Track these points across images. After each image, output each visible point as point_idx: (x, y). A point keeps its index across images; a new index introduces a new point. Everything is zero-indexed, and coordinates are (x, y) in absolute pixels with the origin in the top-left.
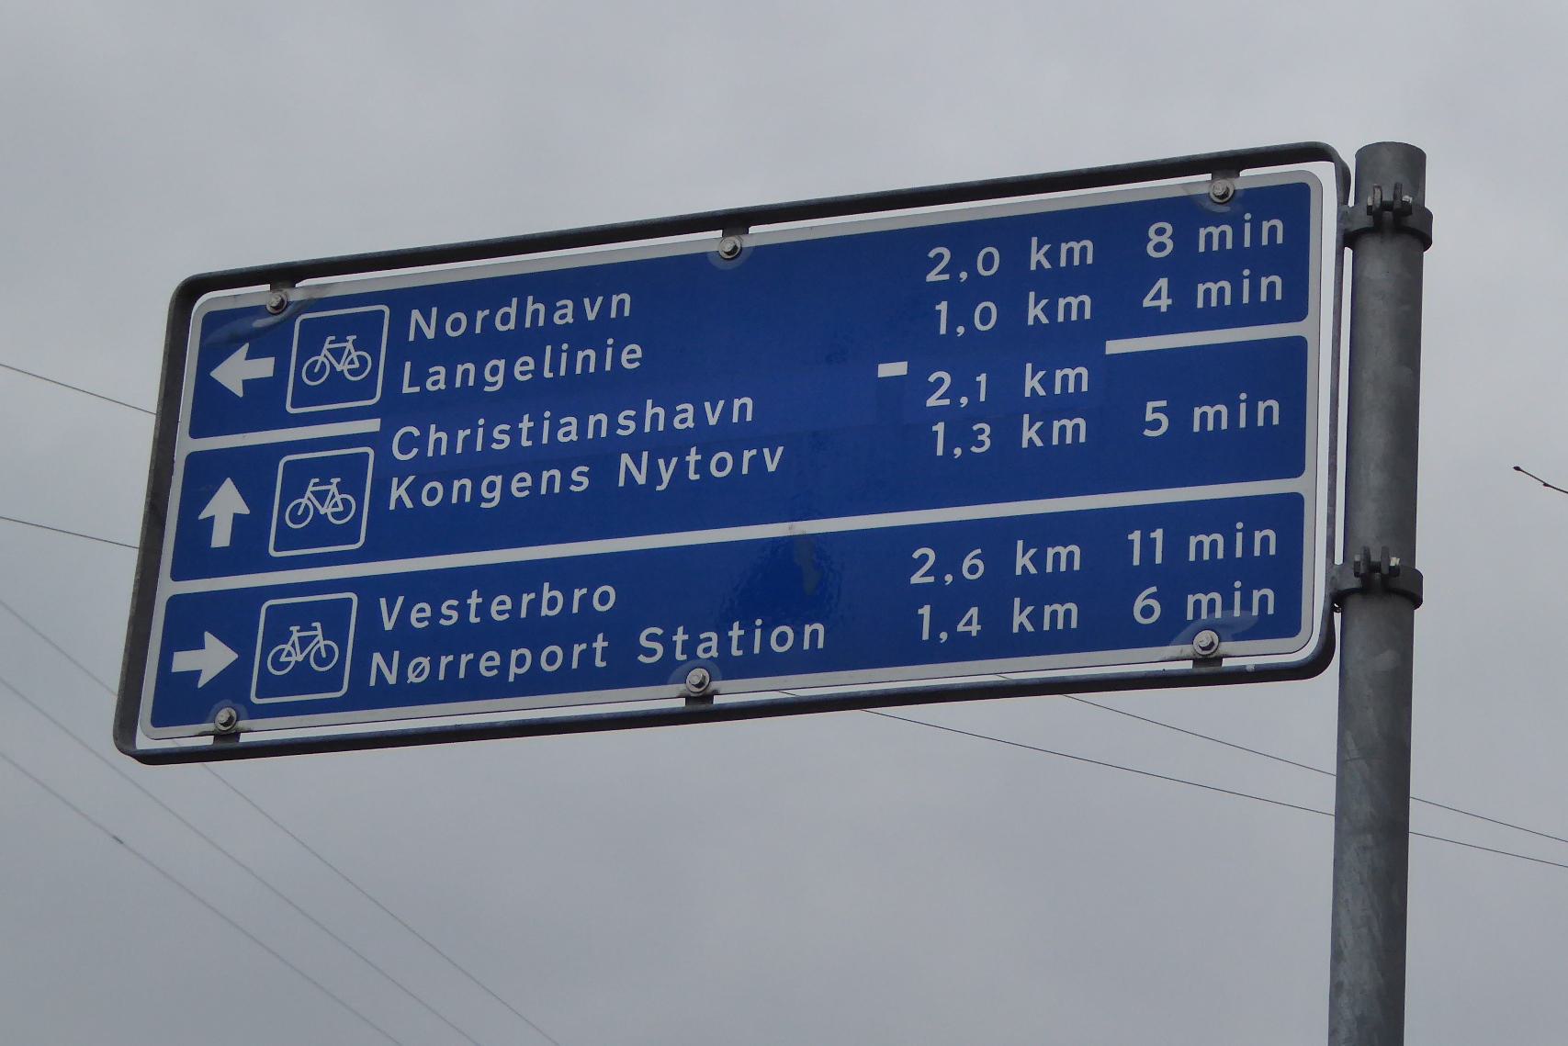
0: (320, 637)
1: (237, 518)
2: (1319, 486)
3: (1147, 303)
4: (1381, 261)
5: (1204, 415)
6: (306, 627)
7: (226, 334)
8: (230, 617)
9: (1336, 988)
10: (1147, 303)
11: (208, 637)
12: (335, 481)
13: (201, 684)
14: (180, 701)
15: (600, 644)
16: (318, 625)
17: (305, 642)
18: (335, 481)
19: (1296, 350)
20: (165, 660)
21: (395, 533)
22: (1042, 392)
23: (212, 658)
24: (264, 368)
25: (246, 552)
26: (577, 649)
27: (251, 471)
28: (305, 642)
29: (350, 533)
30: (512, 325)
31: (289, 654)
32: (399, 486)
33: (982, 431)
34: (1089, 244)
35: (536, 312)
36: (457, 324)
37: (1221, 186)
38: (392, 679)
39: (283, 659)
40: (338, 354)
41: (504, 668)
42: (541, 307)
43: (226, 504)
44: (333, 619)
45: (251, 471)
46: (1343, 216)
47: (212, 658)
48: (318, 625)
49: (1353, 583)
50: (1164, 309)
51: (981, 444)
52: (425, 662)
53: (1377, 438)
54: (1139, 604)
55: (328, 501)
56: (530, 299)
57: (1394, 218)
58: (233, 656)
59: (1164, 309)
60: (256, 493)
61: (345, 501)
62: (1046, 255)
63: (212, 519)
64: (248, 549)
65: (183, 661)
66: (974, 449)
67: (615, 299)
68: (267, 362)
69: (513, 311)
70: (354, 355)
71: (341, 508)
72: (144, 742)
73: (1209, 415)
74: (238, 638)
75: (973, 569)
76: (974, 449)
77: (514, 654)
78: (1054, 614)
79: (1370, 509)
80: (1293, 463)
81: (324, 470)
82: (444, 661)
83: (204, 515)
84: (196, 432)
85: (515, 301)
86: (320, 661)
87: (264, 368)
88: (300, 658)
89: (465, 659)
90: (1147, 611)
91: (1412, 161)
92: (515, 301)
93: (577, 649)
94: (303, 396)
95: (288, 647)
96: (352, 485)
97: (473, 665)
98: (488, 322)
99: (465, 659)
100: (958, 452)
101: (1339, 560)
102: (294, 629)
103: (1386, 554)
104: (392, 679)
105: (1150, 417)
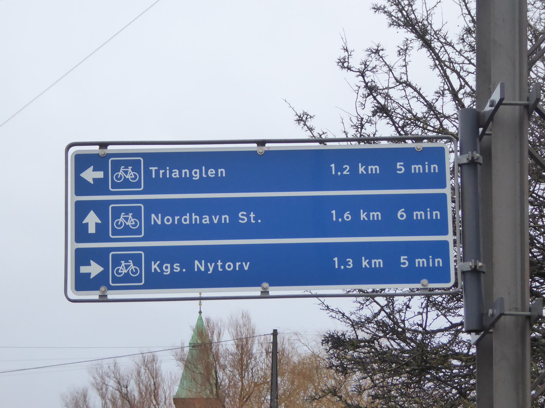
0: (132, 265)
7: (82, 162)
8: (100, 256)
11: (92, 182)
14: (83, 283)
18: (131, 214)
21: (153, 233)
23: (94, 269)
24: (100, 175)
25: (101, 234)
27: (100, 209)
28: (127, 267)
29: (138, 231)
30: (188, 222)
32: (155, 264)
33: (349, 261)
35: (196, 219)
36: (168, 220)
38: (159, 222)
39: (120, 271)
43: (92, 220)
45: (100, 209)
47: (94, 269)
48: (131, 261)
51: (350, 265)
54: (399, 214)
56: (193, 214)
64: (101, 234)
65: (84, 269)
66: (347, 267)
68: (99, 174)
69: (188, 217)
73: (418, 214)
74: (102, 262)
75: (348, 217)
76: (347, 267)
81: (127, 210)
85: (188, 214)
87: (100, 175)
88: (126, 271)
90: (402, 216)
92: (188, 214)
95: (121, 268)
98: (179, 220)
102: (123, 262)
104: (159, 222)
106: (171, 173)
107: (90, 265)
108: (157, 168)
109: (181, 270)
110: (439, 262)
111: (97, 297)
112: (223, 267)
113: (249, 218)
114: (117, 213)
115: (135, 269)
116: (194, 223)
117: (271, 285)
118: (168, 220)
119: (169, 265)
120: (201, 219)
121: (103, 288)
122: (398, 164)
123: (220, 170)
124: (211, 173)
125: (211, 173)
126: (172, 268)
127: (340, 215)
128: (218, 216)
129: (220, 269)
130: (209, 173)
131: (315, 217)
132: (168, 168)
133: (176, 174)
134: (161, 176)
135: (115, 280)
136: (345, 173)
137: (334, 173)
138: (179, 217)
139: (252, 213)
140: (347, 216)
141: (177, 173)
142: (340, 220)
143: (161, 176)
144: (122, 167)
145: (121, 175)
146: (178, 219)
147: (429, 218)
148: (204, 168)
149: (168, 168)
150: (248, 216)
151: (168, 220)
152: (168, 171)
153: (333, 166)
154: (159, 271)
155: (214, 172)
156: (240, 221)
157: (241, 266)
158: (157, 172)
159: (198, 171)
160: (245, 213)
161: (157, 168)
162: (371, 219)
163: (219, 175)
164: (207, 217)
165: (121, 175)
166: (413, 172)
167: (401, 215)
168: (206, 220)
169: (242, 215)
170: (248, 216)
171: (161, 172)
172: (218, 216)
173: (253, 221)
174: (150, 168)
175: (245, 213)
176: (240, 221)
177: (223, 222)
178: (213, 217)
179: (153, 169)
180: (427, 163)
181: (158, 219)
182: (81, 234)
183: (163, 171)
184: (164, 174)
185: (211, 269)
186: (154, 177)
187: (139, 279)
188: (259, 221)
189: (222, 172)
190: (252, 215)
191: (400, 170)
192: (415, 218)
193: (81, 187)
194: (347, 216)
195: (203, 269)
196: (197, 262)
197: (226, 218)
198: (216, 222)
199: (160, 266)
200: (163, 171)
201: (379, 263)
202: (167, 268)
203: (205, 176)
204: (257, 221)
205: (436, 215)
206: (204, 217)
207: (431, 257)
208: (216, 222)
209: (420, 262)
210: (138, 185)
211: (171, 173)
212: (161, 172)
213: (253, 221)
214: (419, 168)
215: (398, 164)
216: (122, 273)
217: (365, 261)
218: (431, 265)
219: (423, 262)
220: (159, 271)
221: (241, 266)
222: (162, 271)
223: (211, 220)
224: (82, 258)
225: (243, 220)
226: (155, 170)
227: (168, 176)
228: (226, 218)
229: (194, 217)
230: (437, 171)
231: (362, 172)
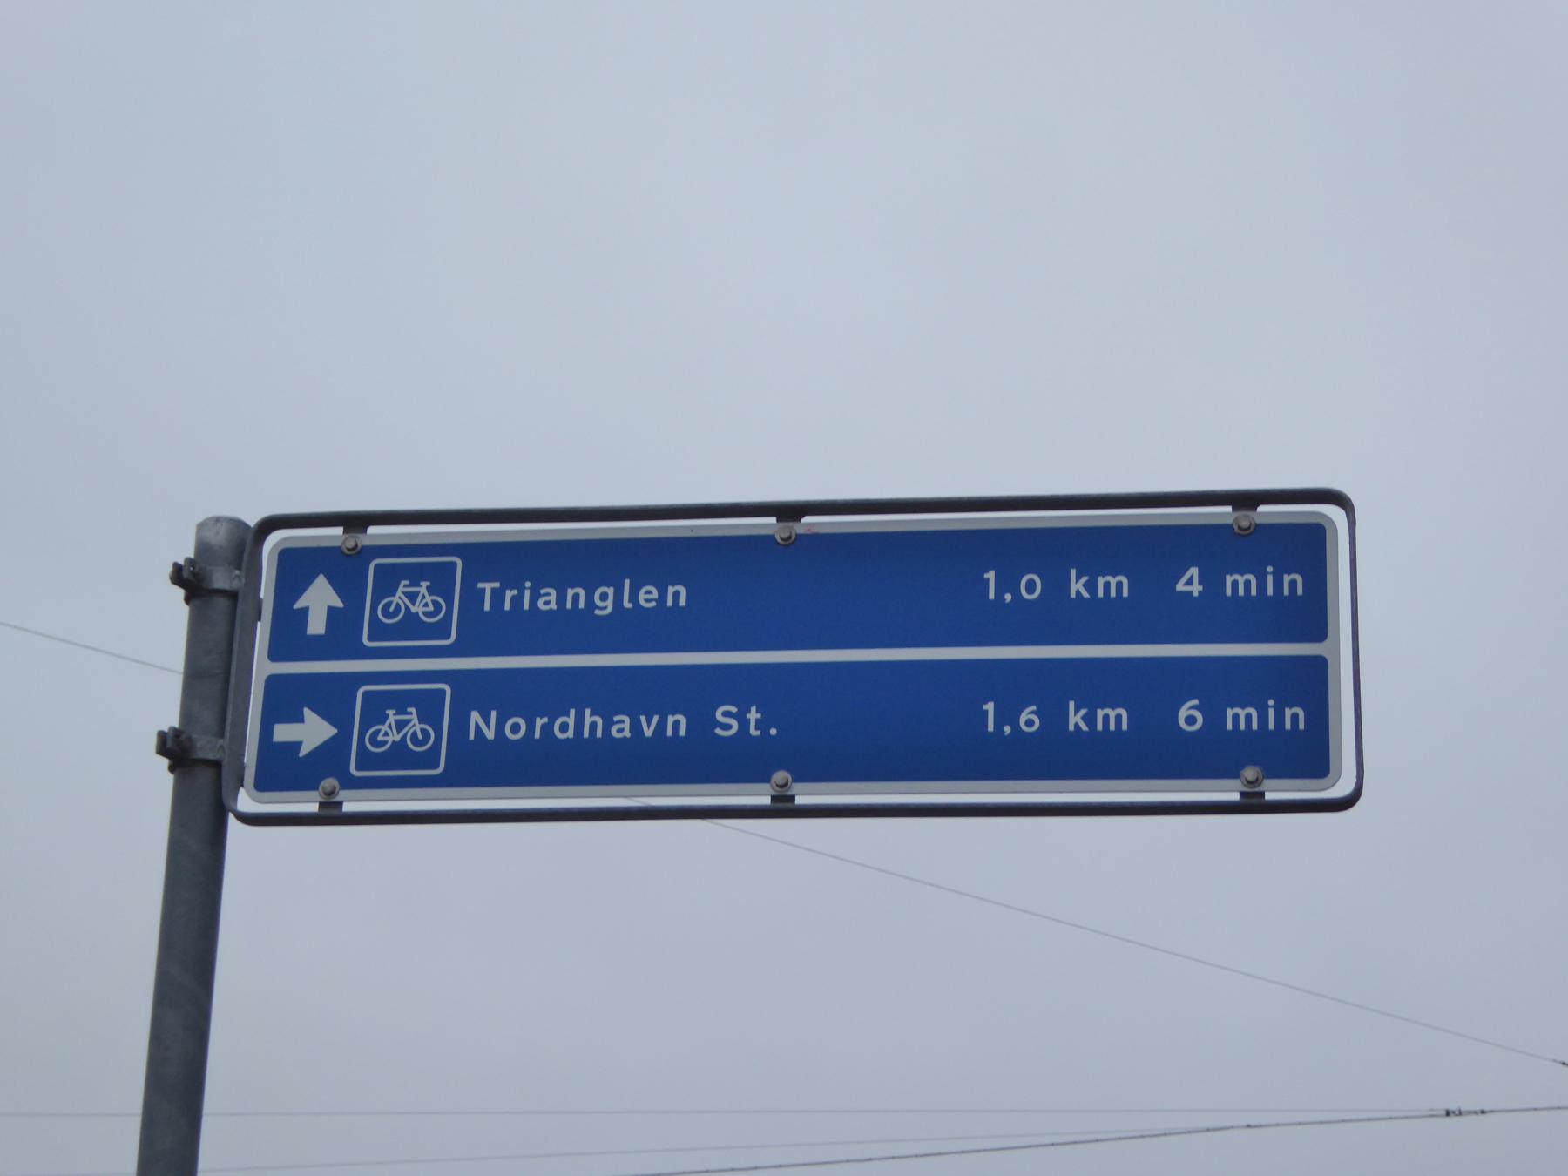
1: (331, 611)
3: (1180, 587)
6: (415, 583)
8: (330, 697)
10: (1180, 587)
11: (307, 712)
12: (425, 584)
16: (413, 710)
17: (400, 725)
23: (312, 731)
28: (400, 725)
29: (442, 630)
30: (570, 734)
31: (386, 734)
34: (1124, 713)
35: (593, 725)
36: (516, 728)
38: (490, 734)
39: (380, 738)
40: (413, 597)
42: (599, 720)
43: (319, 599)
44: (429, 707)
47: (312, 731)
50: (1195, 594)
54: (1183, 713)
56: (588, 711)
58: (333, 731)
59: (1195, 594)
61: (435, 603)
62: (1083, 718)
63: (305, 611)
64: (342, 635)
65: (283, 733)
67: (671, 720)
69: (571, 720)
70: (428, 599)
71: (431, 608)
74: (336, 712)
75: (1030, 723)
78: (1107, 585)
83: (298, 605)
84: (275, 655)
85: (572, 712)
88: (397, 738)
90: (1191, 720)
92: (572, 712)
95: (384, 728)
98: (547, 729)
102: (390, 712)
104: (490, 734)
106: (535, 597)
107: (301, 720)
108: (497, 585)
110: (1293, 583)
113: (744, 723)
115: (423, 731)
116: (586, 735)
118: (516, 728)
120: (608, 724)
123: (671, 590)
124: (648, 596)
125: (648, 596)
127: (1007, 714)
128: (656, 718)
130: (642, 597)
132: (528, 584)
133: (548, 600)
134: (507, 607)
135: (366, 760)
138: (545, 720)
139: (753, 709)
141: (553, 598)
142: (1008, 597)
143: (507, 607)
144: (404, 582)
145: (398, 605)
146: (543, 726)
147: (1271, 726)
148: (627, 582)
149: (528, 584)
151: (516, 728)
152: (527, 593)
153: (991, 576)
155: (655, 595)
156: (718, 731)
158: (498, 596)
159: (610, 591)
160: (734, 709)
161: (497, 585)
162: (1100, 727)
163: (670, 603)
164: (627, 719)
165: (398, 605)
166: (1229, 726)
167: (1190, 583)
171: (509, 594)
172: (656, 718)
173: (754, 732)
174: (480, 585)
175: (734, 709)
176: (718, 731)
177: (669, 733)
178: (643, 719)
179: (488, 587)
180: (1271, 702)
181: (488, 725)
183: (515, 592)
184: (516, 601)
186: (487, 607)
187: (430, 759)
188: (773, 732)
189: (677, 595)
190: (753, 715)
192: (1229, 726)
194: (1029, 720)
197: (678, 722)
198: (648, 733)
200: (515, 592)
201: (1119, 585)
203: (630, 606)
204: (765, 732)
205: (1293, 583)
206: (616, 718)
207: (1271, 702)
208: (648, 733)
209: (1239, 716)
210: (442, 630)
211: (535, 597)
212: (509, 594)
213: (754, 732)
214: (1248, 717)
216: (385, 743)
217: (1076, 712)
218: (1271, 726)
223: (636, 727)
225: (728, 727)
226: (493, 590)
227: (526, 607)
228: (678, 722)
229: (588, 719)
231: (1078, 592)
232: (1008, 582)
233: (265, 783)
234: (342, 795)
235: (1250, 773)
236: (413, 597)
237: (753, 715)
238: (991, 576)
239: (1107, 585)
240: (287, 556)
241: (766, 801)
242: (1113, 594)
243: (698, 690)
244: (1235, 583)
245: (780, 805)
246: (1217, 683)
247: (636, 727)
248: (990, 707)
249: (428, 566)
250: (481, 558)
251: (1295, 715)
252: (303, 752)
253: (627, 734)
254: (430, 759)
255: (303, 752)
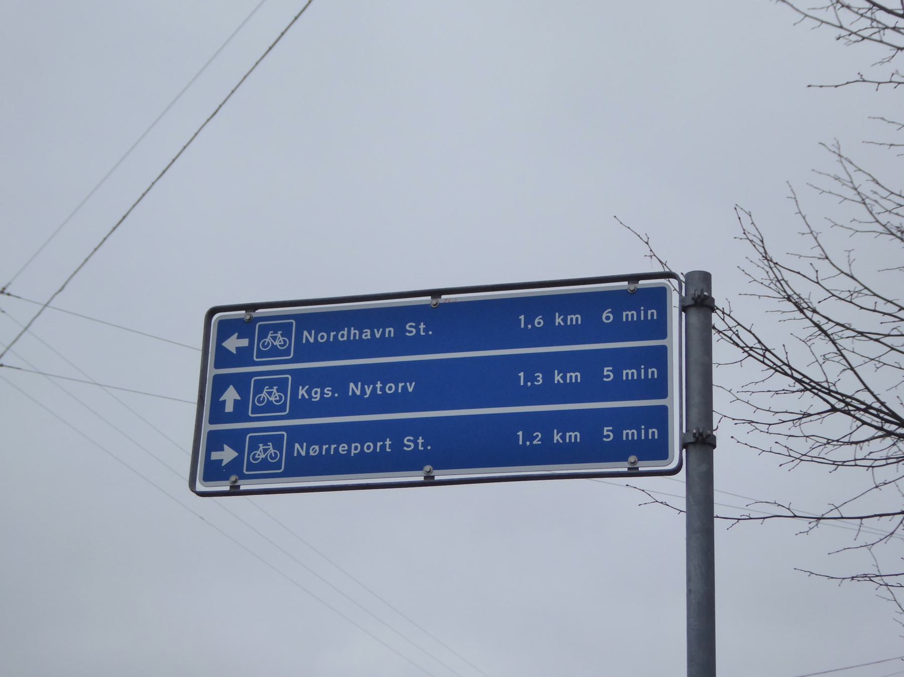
2: (675, 402)
4: (695, 316)
5: (627, 434)
7: (226, 328)
8: (235, 439)
9: (689, 592)
12: (275, 388)
13: (223, 464)
14: (214, 471)
15: (388, 442)
17: (265, 451)
18: (275, 388)
19: (664, 410)
20: (208, 455)
21: (305, 352)
22: (562, 382)
23: (227, 455)
24: (245, 342)
25: (240, 413)
26: (379, 444)
28: (265, 451)
29: (282, 408)
30: (345, 338)
35: (355, 334)
36: (323, 337)
37: (632, 287)
38: (303, 453)
40: (270, 394)
41: (349, 450)
42: (357, 332)
43: (231, 396)
44: (277, 442)
46: (682, 300)
47: (227, 455)
49: (692, 440)
51: (538, 381)
52: (317, 447)
53: (696, 383)
55: (273, 396)
57: (700, 302)
58: (236, 454)
60: (243, 390)
61: (284, 341)
63: (225, 401)
64: (240, 413)
65: (215, 456)
67: (387, 330)
69: (345, 333)
70: (277, 394)
72: (200, 487)
73: (629, 373)
74: (237, 446)
75: (539, 323)
77: (353, 445)
78: (572, 319)
79: (694, 411)
80: (663, 393)
82: (325, 447)
86: (272, 458)
87: (245, 342)
88: (264, 456)
89: (333, 447)
91: (706, 278)
93: (379, 444)
94: (261, 354)
95: (258, 452)
96: (282, 389)
97: (336, 449)
98: (336, 337)
99: (333, 447)
100: (529, 384)
101: (684, 431)
103: (702, 291)
104: (312, 340)
105: (605, 373)
107: (222, 449)
109: (333, 394)
110: (653, 433)
111: (227, 488)
112: (382, 389)
113: (416, 444)
114: (259, 388)
117: (436, 467)
118: (323, 337)
119: (319, 390)
121: (233, 478)
122: (606, 429)
126: (322, 393)
129: (379, 392)
131: (495, 382)
135: (251, 467)
136: (535, 442)
137: (523, 326)
140: (539, 322)
142: (530, 326)
150: (417, 328)
151: (322, 337)
153: (522, 317)
154: (307, 397)
157: (405, 388)
166: (624, 438)
167: (607, 316)
168: (367, 334)
169: (410, 326)
170: (417, 328)
173: (421, 448)
181: (311, 335)
182: (218, 414)
185: (368, 392)
187: (277, 466)
190: (420, 441)
191: (608, 436)
192: (624, 438)
193: (223, 358)
194: (539, 322)
195: (358, 393)
196: (352, 385)
197: (390, 331)
198: (378, 336)
199: (309, 392)
202: (316, 393)
208: (378, 336)
209: (629, 434)
214: (632, 315)
215: (606, 429)
219: (633, 373)
220: (307, 397)
221: (405, 388)
222: (311, 397)
223: (373, 334)
224: (216, 441)
229: (353, 332)
230: (656, 376)
232: (530, 320)
233: (207, 478)
234: (240, 482)
235: (632, 459)
236: (274, 338)
237: (420, 441)
238: (522, 317)
239: (571, 377)
240: (222, 323)
241: (422, 479)
242: (574, 381)
243: (398, 430)
244: (627, 374)
245: (427, 481)
246: (620, 359)
247: (373, 334)
248: (520, 433)
249: (281, 326)
250: (305, 321)
251: (654, 432)
252: (236, 335)
253: (369, 337)
254: (282, 408)
255: (236, 335)
